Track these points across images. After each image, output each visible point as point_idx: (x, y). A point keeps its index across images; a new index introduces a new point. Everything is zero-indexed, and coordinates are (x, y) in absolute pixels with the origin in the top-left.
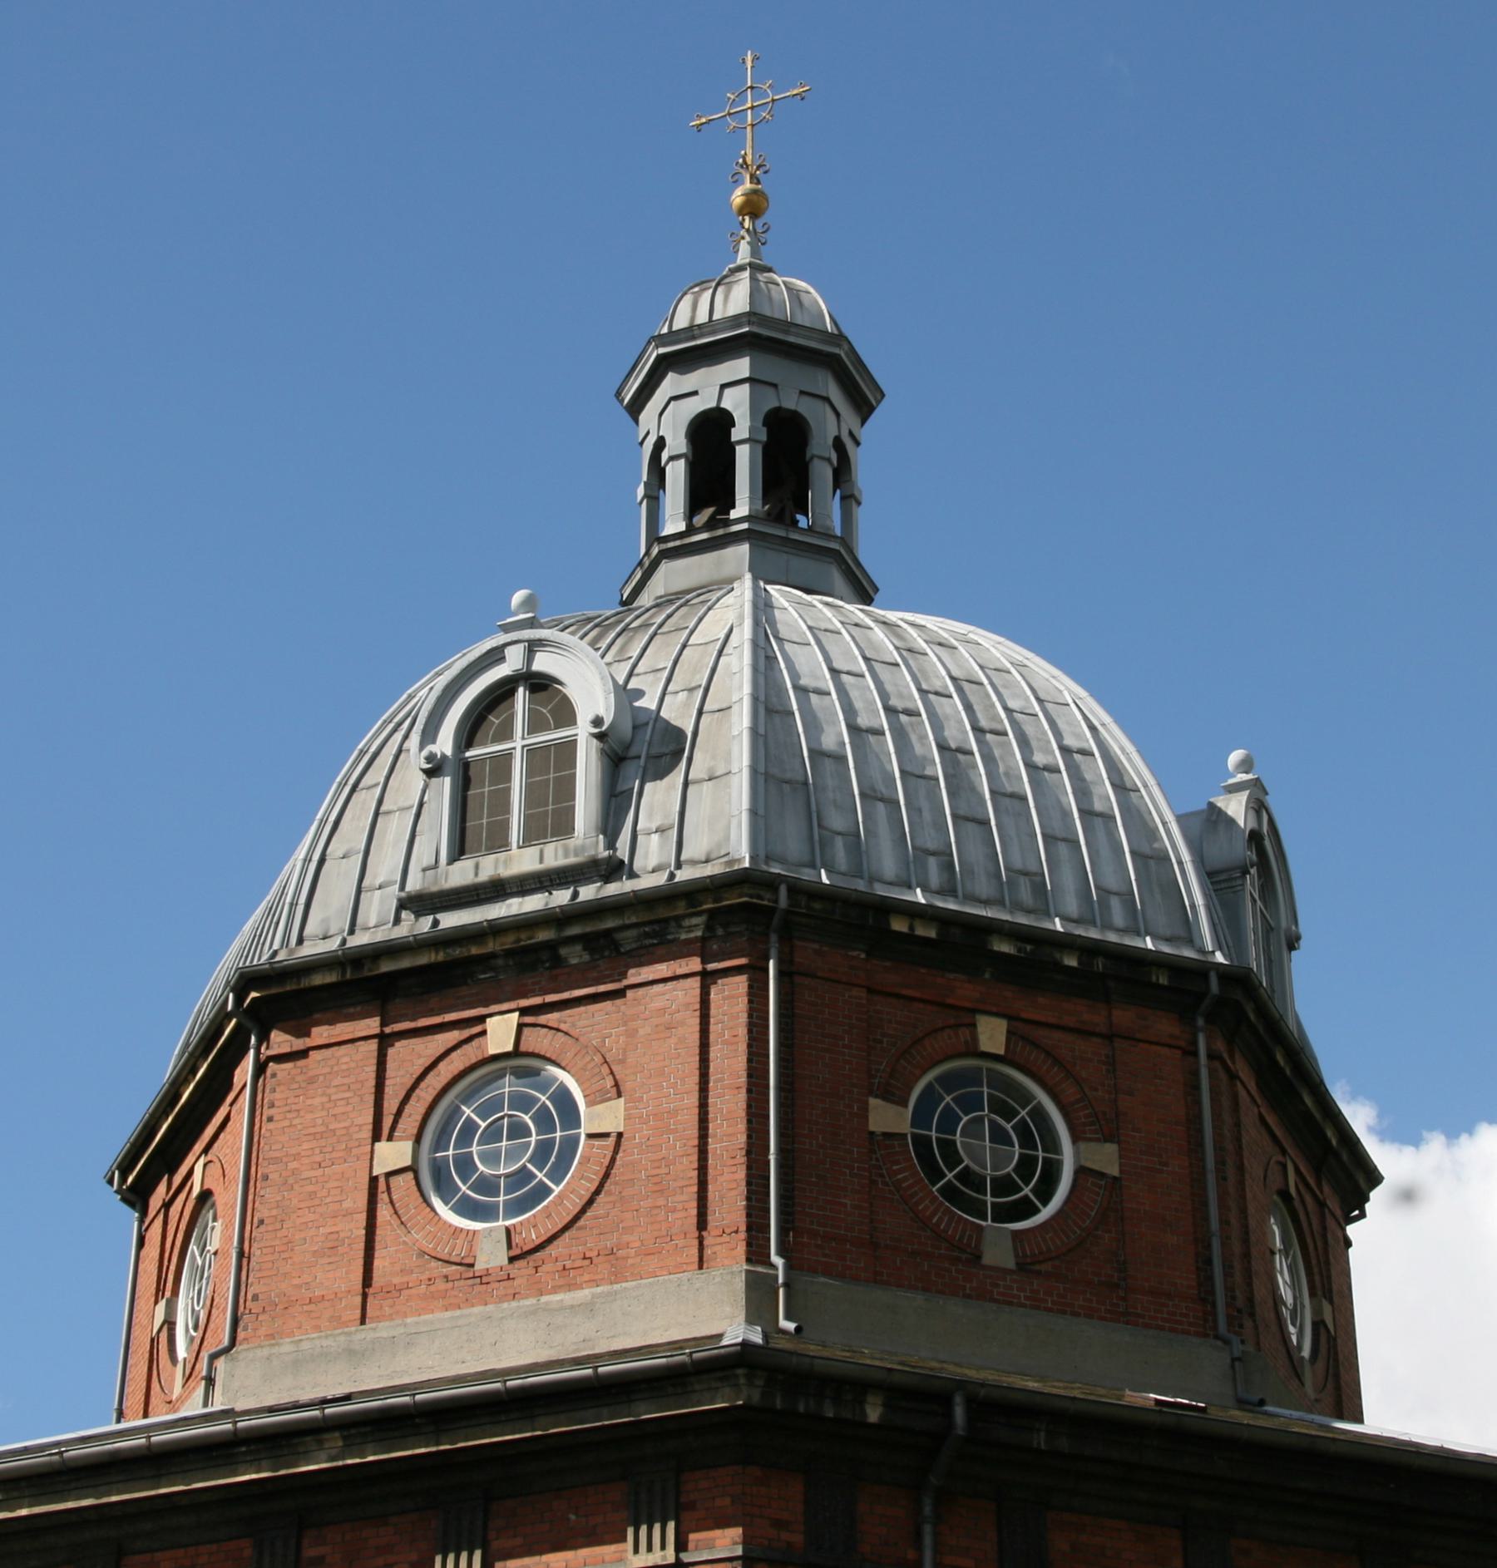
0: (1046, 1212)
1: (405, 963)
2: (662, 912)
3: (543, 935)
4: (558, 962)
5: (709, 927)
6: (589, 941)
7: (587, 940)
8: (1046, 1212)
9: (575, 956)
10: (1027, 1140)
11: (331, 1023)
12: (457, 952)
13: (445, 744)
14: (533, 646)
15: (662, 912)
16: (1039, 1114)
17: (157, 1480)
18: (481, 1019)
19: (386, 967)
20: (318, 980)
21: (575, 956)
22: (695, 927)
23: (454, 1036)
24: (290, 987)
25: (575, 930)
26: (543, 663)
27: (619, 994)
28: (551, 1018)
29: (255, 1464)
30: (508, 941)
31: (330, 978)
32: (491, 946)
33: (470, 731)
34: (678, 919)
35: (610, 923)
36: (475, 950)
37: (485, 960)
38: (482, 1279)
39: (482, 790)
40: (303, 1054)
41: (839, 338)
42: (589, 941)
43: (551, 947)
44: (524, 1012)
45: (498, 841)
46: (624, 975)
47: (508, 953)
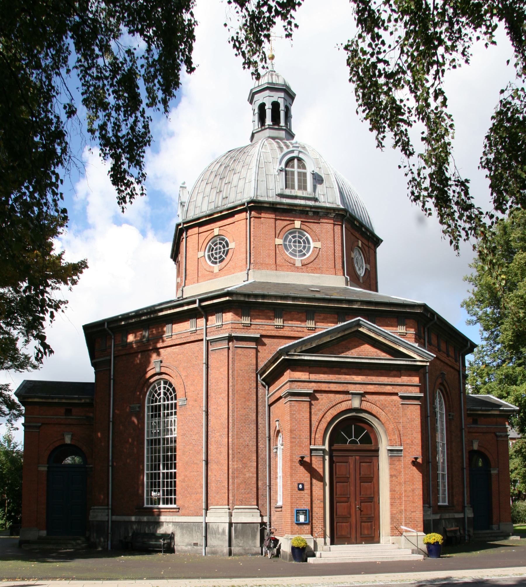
0: (308, 255)
1: (282, 207)
2: (329, 211)
3: (308, 209)
4: (307, 214)
5: (335, 216)
6: (314, 213)
7: (314, 212)
8: (308, 255)
9: (311, 214)
10: (304, 243)
11: (266, 213)
12: (292, 208)
13: (283, 165)
14: (300, 152)
15: (329, 211)
16: (307, 238)
17: (329, 303)
18: (294, 221)
19: (278, 206)
20: (265, 205)
21: (311, 214)
22: (333, 215)
23: (289, 222)
24: (260, 205)
25: (313, 210)
26: (301, 156)
27: (319, 223)
28: (307, 224)
29: (345, 304)
30: (301, 208)
31: (268, 205)
32: (298, 208)
33: (287, 165)
34: (331, 213)
35: (320, 210)
36: (295, 208)
37: (295, 210)
38: (297, 267)
39: (289, 177)
40: (260, 218)
41: (285, 85)
42: (314, 213)
43: (308, 211)
44: (302, 221)
45: (293, 188)
46: (319, 220)
47: (300, 210)
